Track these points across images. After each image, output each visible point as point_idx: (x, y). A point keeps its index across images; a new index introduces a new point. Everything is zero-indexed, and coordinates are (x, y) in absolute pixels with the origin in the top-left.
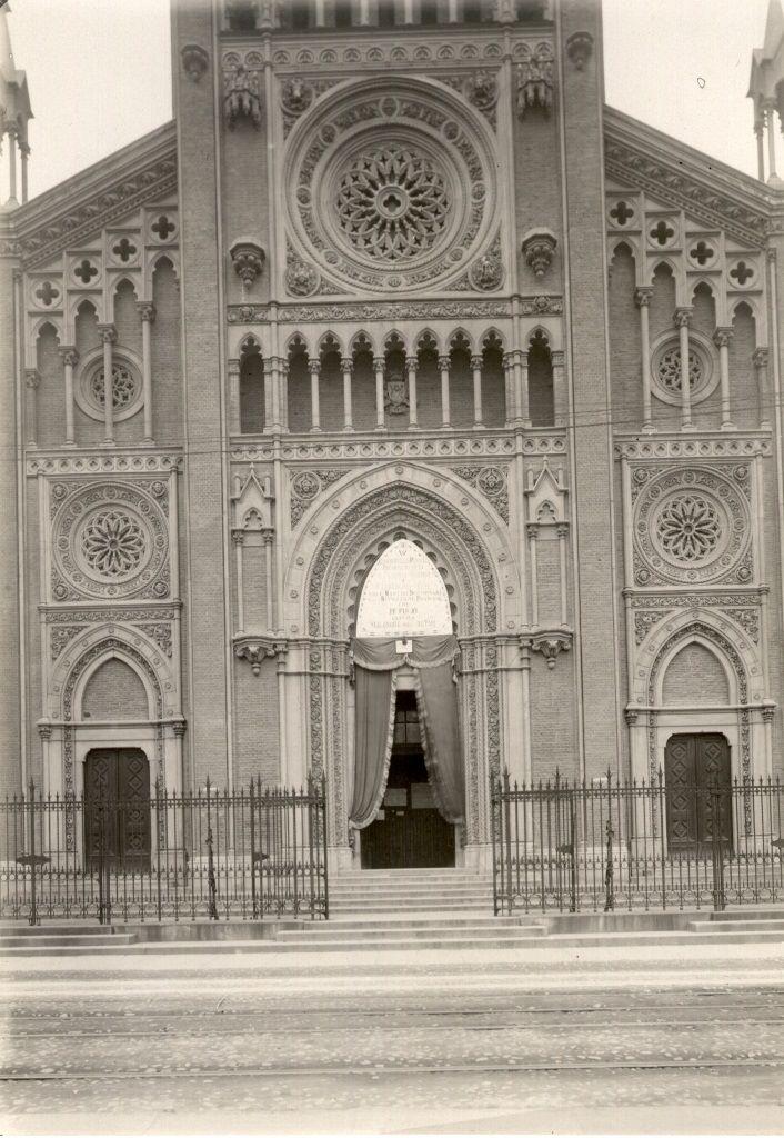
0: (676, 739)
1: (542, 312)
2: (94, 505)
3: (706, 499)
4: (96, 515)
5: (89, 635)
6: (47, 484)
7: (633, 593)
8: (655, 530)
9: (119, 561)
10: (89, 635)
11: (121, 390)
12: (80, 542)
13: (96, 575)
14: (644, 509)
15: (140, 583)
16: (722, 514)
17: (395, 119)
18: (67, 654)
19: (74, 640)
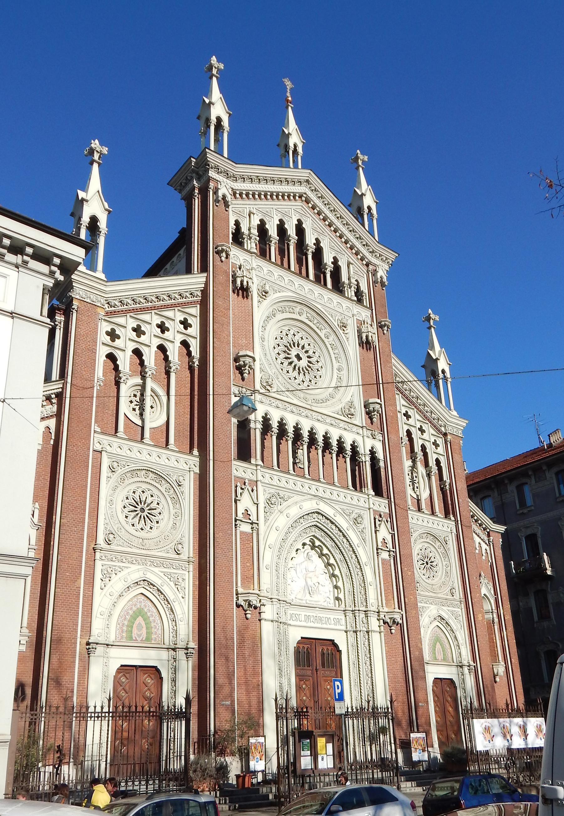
0: (124, 669)
3: (155, 492)
7: (161, 562)
8: (120, 506)
9: (134, 517)
14: (115, 489)
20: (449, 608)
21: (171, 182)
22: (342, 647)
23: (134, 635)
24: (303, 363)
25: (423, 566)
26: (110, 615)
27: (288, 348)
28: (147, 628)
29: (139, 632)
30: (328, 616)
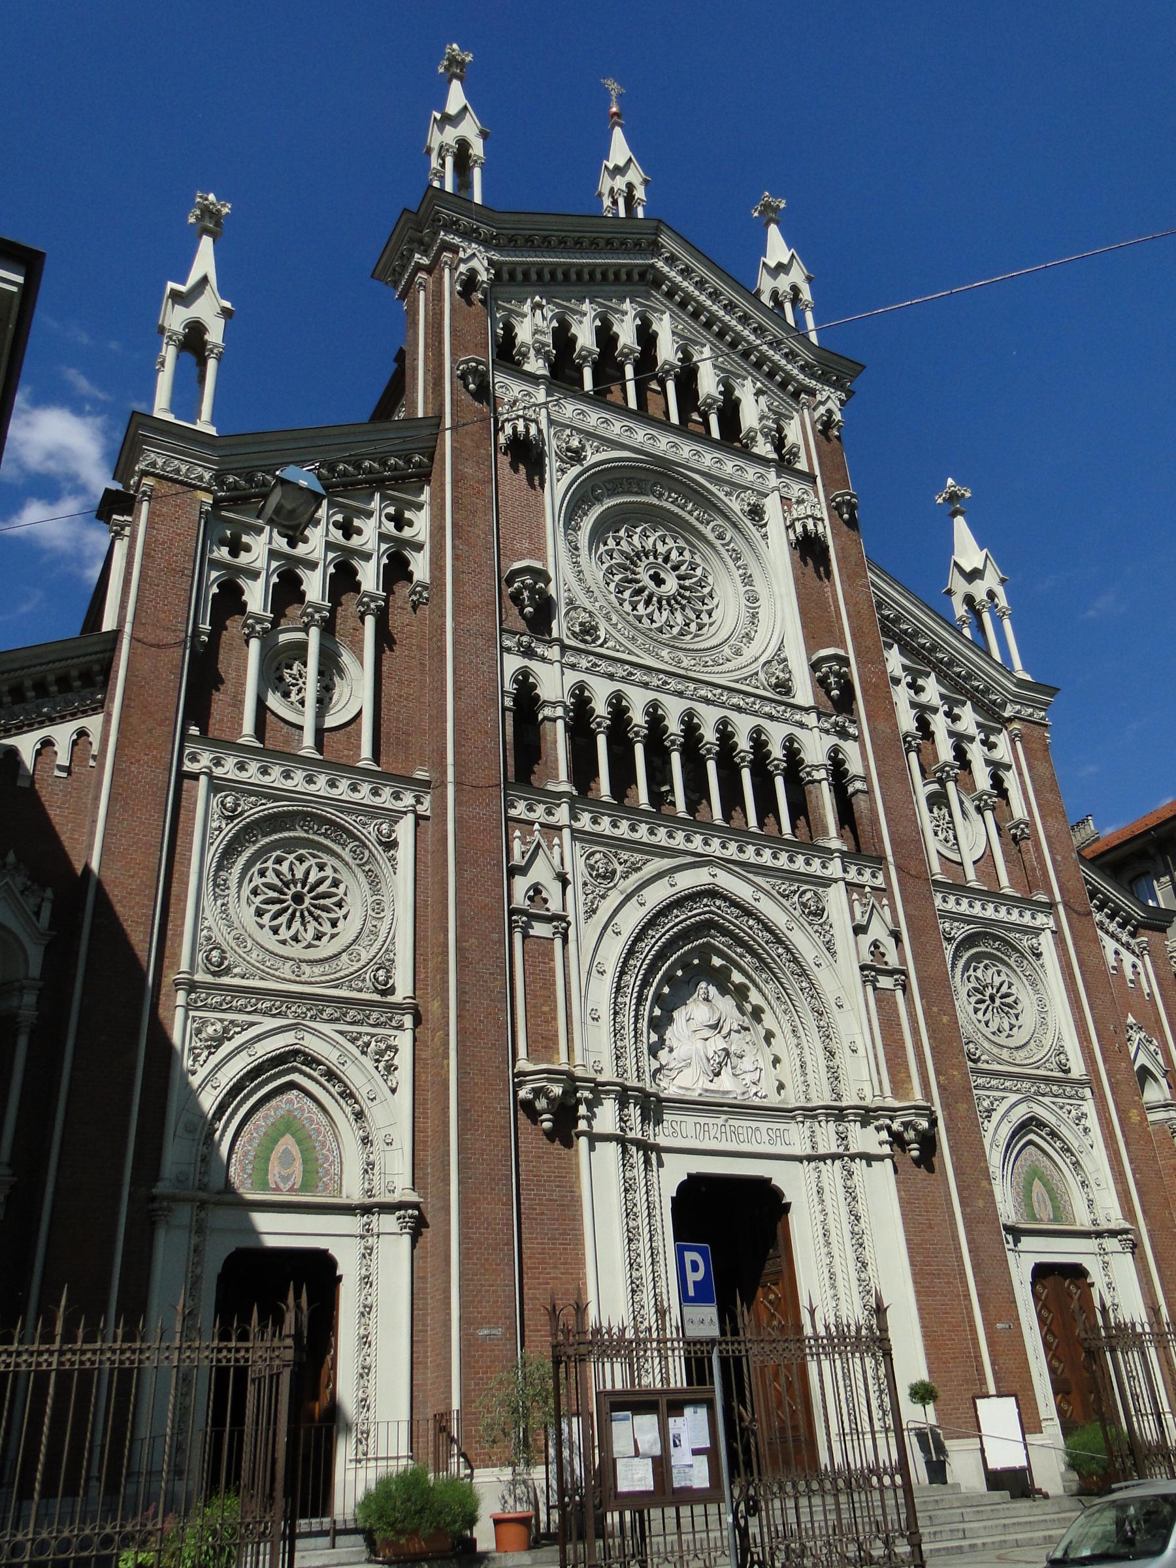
13: (267, 938)
15: (346, 965)
16: (357, 891)
21: (377, 272)
23: (273, 1178)
24: (671, 585)
25: (1004, 989)
28: (305, 1162)
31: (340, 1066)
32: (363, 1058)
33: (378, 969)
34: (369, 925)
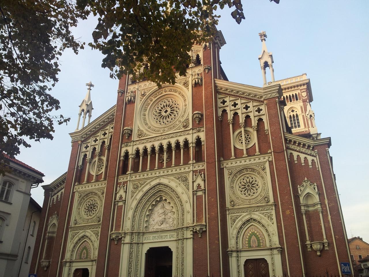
1: (199, 132)
2: (241, 175)
4: (242, 177)
5: (243, 217)
6: (78, 193)
9: (251, 191)
10: (243, 217)
11: (247, 139)
12: (237, 187)
13: (243, 196)
15: (259, 198)
17: (167, 93)
18: (74, 240)
19: (76, 236)
20: (91, 230)
22: (173, 249)
23: (82, 257)
24: (163, 114)
26: (269, 235)
27: (172, 110)
29: (254, 244)
30: (166, 235)
31: (260, 220)
32: (265, 218)
33: (265, 198)
34: (263, 188)
